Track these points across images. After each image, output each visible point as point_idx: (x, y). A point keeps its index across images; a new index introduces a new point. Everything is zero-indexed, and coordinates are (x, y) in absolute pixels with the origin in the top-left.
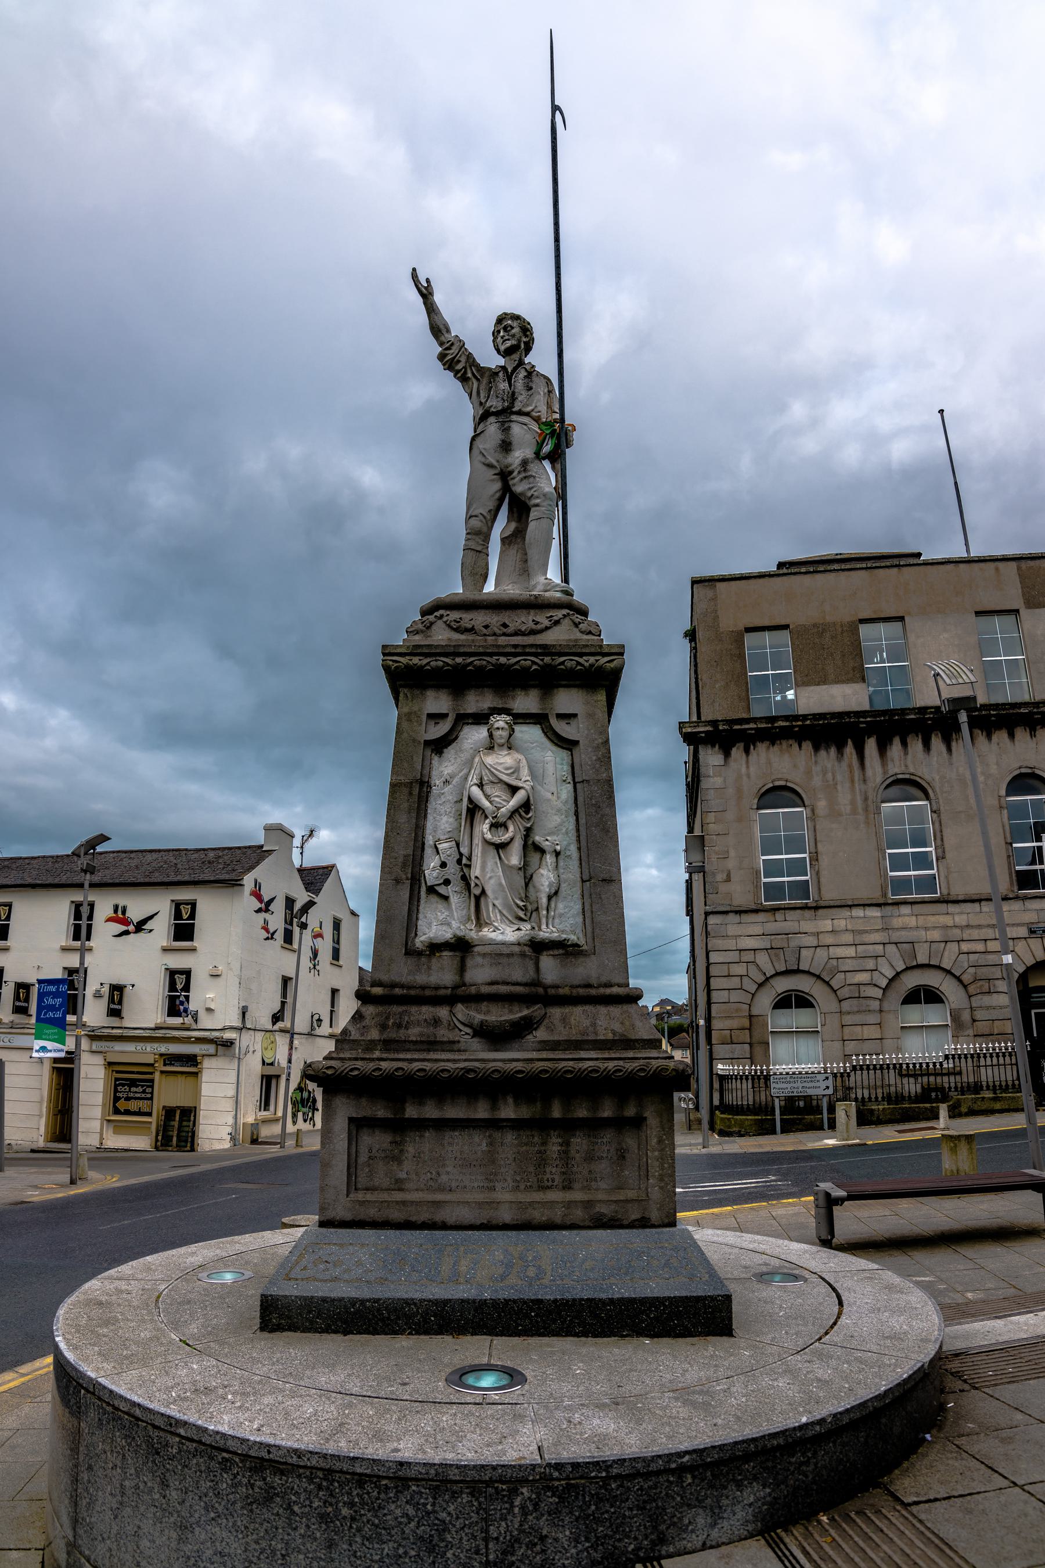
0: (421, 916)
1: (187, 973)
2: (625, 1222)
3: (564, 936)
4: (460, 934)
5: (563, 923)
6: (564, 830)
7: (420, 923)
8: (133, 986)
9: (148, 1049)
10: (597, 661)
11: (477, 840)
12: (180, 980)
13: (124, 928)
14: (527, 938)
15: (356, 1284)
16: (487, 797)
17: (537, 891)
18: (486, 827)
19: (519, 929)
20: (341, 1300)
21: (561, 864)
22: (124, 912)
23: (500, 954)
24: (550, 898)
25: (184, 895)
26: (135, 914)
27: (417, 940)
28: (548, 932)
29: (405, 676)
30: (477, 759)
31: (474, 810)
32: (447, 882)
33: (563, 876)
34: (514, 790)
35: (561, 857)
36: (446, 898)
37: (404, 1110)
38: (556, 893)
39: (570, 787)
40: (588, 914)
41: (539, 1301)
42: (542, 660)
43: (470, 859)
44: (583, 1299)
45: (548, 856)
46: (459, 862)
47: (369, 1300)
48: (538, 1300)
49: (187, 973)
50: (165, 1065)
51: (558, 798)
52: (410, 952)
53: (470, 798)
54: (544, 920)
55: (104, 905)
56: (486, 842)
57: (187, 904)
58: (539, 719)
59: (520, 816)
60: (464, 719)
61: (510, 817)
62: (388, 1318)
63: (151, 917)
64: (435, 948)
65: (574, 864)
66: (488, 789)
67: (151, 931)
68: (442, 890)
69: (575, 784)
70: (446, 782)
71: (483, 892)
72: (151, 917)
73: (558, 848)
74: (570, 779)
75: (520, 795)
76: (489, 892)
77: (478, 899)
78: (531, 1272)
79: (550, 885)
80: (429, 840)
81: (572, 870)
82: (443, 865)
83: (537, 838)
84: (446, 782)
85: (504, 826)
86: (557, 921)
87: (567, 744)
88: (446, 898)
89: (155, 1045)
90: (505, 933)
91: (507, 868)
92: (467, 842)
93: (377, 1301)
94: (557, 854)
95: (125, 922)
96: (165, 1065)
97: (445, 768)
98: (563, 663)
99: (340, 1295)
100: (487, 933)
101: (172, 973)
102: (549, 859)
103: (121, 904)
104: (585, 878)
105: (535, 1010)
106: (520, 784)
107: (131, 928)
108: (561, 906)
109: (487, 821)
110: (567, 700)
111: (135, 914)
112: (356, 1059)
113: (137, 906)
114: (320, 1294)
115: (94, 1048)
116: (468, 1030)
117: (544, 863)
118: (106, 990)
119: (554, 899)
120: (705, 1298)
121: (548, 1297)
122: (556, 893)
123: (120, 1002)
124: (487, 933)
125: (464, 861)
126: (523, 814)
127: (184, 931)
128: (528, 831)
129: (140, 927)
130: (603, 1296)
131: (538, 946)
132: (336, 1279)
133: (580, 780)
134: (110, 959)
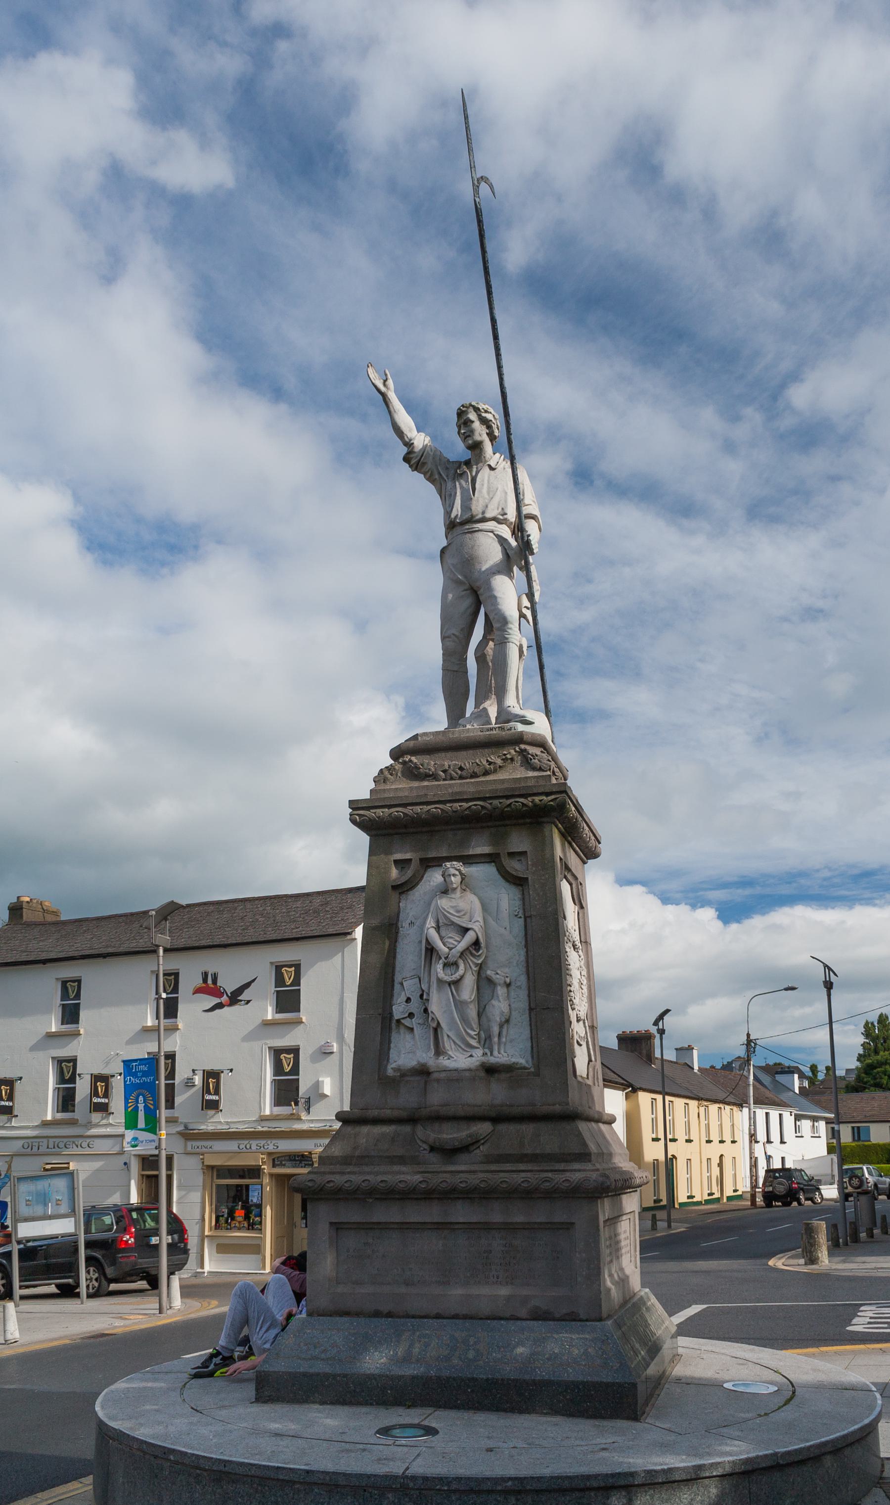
0: (392, 1045)
1: (295, 1051)
2: (557, 1316)
3: (513, 1060)
4: (423, 1061)
5: (513, 1051)
6: (515, 962)
8: (231, 1070)
9: (254, 1147)
10: (541, 801)
11: (434, 979)
12: (287, 1062)
13: (216, 1001)
14: (478, 1063)
15: (330, 1362)
16: (442, 938)
17: (489, 1021)
19: (471, 1056)
20: (318, 1374)
21: (512, 994)
22: (215, 981)
23: (456, 1078)
24: (501, 1026)
25: (285, 954)
26: (229, 984)
27: (390, 1067)
28: (500, 1057)
30: (434, 903)
31: (431, 951)
32: (411, 1015)
33: (513, 1006)
35: (513, 987)
36: (412, 1029)
38: (507, 1021)
39: (522, 919)
41: (474, 1380)
42: (491, 804)
43: (428, 994)
44: (510, 1379)
45: (499, 988)
46: (421, 996)
47: (339, 1375)
48: (473, 1379)
49: (295, 1051)
50: (274, 1166)
53: (427, 940)
54: (496, 1047)
55: (191, 971)
56: (440, 981)
57: (290, 966)
58: (492, 858)
59: (472, 954)
60: (428, 863)
62: (354, 1391)
63: (248, 985)
64: (404, 1074)
65: (523, 994)
67: (248, 1002)
68: (407, 1022)
69: (525, 918)
72: (248, 985)
75: (470, 937)
77: (436, 1030)
78: (471, 1354)
79: (502, 1013)
80: (398, 978)
82: (408, 1000)
83: (489, 972)
87: (518, 882)
88: (412, 1029)
89: (262, 1142)
90: (460, 1059)
91: (460, 1005)
92: (426, 980)
93: (345, 1376)
94: (508, 985)
95: (216, 991)
96: (274, 1166)
98: (510, 805)
99: (316, 1371)
100: (444, 1062)
101: (277, 1053)
103: (211, 972)
104: (533, 1006)
105: (484, 1128)
106: (470, 926)
107: (224, 999)
108: (511, 1032)
109: (441, 961)
110: (519, 841)
111: (229, 984)
112: (334, 1173)
113: (231, 970)
114: (302, 1370)
115: (189, 1149)
116: (425, 1146)
118: (198, 1080)
120: (613, 1384)
121: (481, 1376)
122: (507, 1021)
123: (217, 1092)
125: (425, 997)
126: (474, 952)
127: (288, 1001)
128: (481, 966)
129: (234, 999)
130: (527, 1377)
131: (490, 1070)
132: (315, 1358)
134: (202, 1038)
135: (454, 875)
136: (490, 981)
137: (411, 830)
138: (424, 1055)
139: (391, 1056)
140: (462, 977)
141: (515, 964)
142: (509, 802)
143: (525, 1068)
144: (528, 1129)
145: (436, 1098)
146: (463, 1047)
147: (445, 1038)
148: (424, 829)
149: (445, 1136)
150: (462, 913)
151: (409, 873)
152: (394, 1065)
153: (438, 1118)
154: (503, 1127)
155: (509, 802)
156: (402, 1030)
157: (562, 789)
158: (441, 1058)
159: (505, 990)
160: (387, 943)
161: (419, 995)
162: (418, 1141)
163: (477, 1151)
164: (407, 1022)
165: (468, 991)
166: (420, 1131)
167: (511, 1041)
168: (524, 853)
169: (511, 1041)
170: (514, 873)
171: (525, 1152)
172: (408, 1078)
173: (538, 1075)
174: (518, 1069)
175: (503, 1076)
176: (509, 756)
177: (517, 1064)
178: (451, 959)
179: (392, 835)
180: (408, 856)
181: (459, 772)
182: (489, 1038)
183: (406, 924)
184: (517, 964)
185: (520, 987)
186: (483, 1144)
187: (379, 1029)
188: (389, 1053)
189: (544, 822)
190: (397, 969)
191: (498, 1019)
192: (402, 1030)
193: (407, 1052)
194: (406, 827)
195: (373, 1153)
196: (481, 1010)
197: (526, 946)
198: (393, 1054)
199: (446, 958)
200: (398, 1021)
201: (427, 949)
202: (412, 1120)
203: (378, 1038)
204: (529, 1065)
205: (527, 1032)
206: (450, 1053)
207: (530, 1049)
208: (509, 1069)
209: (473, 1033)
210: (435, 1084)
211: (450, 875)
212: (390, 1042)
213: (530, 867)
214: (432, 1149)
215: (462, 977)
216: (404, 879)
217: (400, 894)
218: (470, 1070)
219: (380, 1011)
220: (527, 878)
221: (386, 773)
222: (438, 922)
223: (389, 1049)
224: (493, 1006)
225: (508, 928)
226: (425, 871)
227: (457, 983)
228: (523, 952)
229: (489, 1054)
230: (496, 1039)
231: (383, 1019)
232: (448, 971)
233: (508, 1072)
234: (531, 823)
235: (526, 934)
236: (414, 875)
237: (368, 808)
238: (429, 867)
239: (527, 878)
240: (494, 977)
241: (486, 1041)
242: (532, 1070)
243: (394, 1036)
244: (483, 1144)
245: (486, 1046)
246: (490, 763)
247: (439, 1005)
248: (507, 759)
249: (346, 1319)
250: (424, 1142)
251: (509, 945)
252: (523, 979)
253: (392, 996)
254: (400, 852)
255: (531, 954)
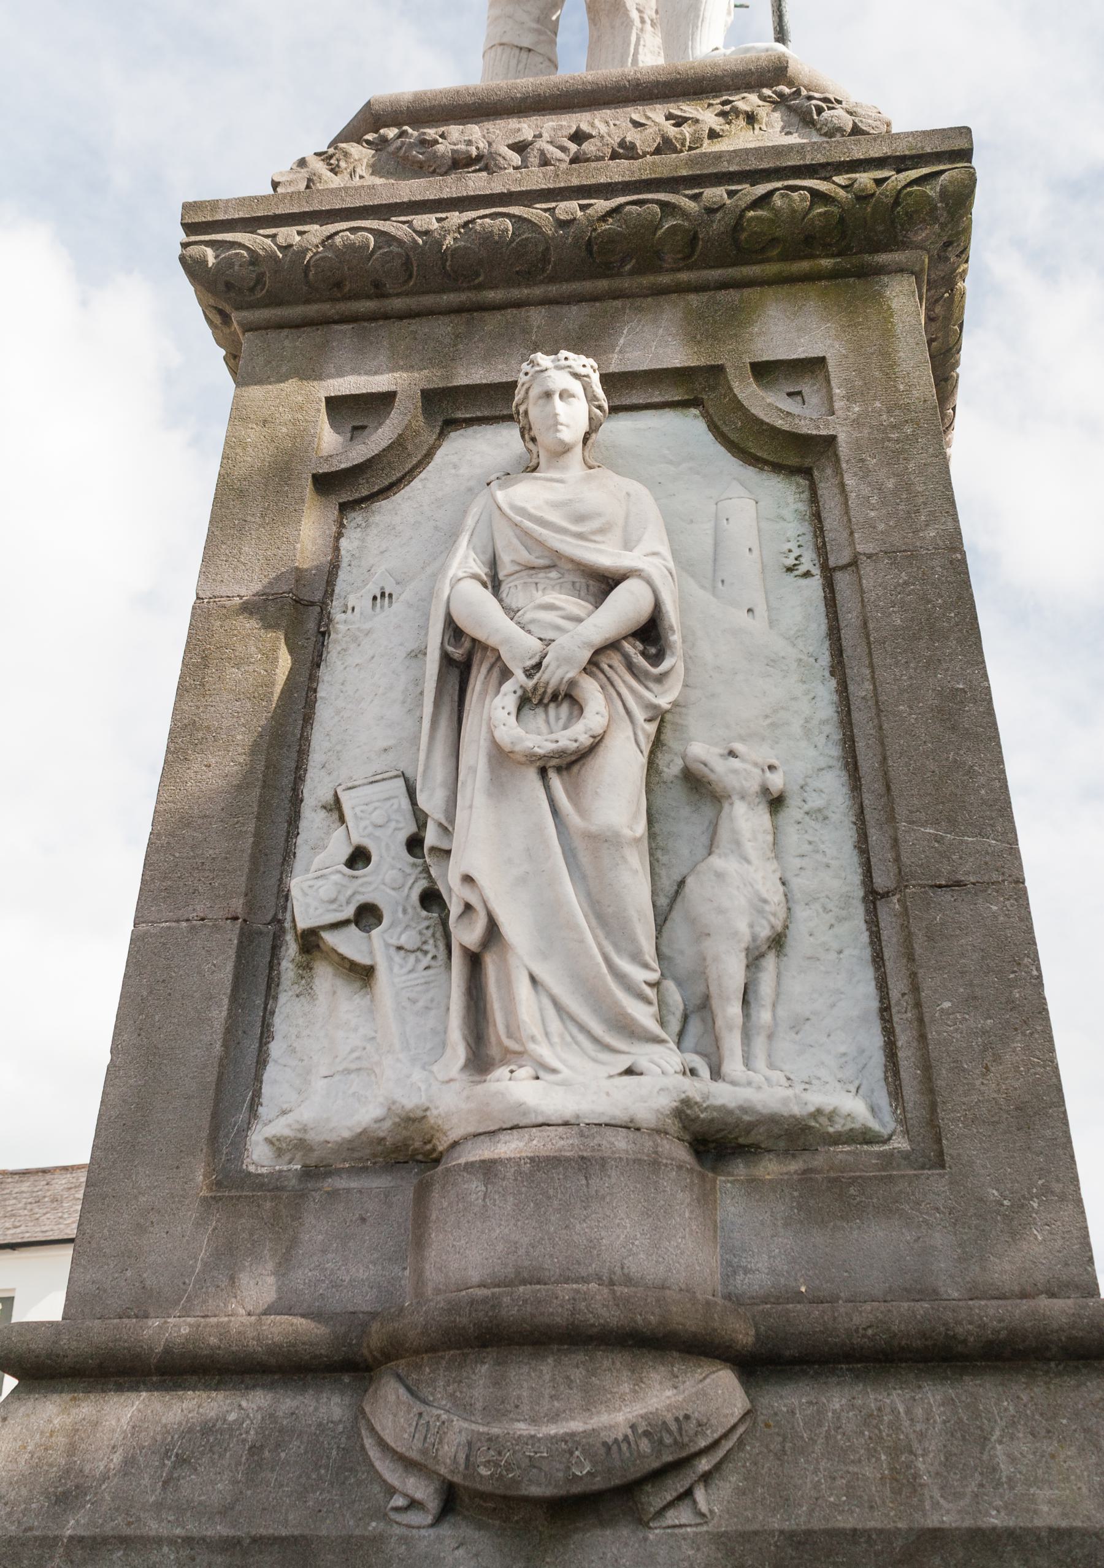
0: (276, 1048)
4: (410, 1101)
5: (813, 1059)
7: (271, 1073)
10: (879, 182)
16: (511, 612)
17: (702, 934)
18: (506, 700)
21: (792, 837)
24: (754, 961)
28: (758, 1084)
29: (265, 289)
31: (463, 661)
32: (367, 915)
33: (795, 883)
34: (603, 583)
35: (792, 811)
36: (362, 974)
37: (14, 1375)
38: (778, 942)
39: (814, 586)
40: (902, 1018)
43: (446, 831)
46: (414, 844)
51: (772, 623)
52: (232, 1186)
54: (732, 1043)
56: (502, 758)
58: (691, 388)
59: (630, 667)
61: (593, 665)
64: (317, 1169)
65: (837, 841)
66: (516, 593)
68: (348, 944)
69: (829, 574)
70: (383, 596)
71: (493, 931)
73: (776, 782)
74: (809, 561)
75: (625, 606)
76: (513, 928)
77: (474, 961)
80: (316, 789)
81: (826, 862)
82: (359, 857)
84: (383, 596)
85: (567, 697)
86: (785, 1044)
87: (795, 456)
90: (574, 1078)
91: (584, 852)
92: (440, 771)
94: (776, 803)
97: (382, 544)
100: (517, 1088)
102: (747, 820)
109: (508, 686)
110: (788, 329)
117: (724, 834)
119: (770, 962)
122: (778, 942)
124: (517, 1088)
125: (431, 838)
131: (715, 1143)
133: (845, 558)
135: (565, 395)
136: (698, 785)
137: (398, 304)
138: (418, 1075)
139: (266, 1089)
140: (596, 744)
141: (796, 728)
142: (761, 189)
143: (866, 1137)
144: (920, 1408)
145: (470, 1252)
146: (598, 1029)
147: (523, 989)
148: (449, 299)
149: (522, 1428)
150: (595, 524)
151: (380, 437)
152: (271, 1131)
153: (497, 1335)
154: (791, 1400)
155: (761, 189)
156: (324, 977)
157: (958, 144)
158: (502, 1072)
159: (762, 817)
160: (285, 661)
161: (403, 836)
162: (374, 1453)
163: (682, 1515)
164: (348, 944)
165: (617, 792)
166: (392, 1412)
167: (797, 1025)
168: (814, 366)
169: (797, 1025)
170: (779, 423)
171: (933, 1521)
172: (341, 1183)
173: (940, 1163)
174: (837, 1139)
175: (770, 1168)
176: (742, 106)
177: (832, 1116)
178: (554, 674)
179: (327, 321)
180: (380, 383)
181: (573, 147)
182: (701, 1008)
183: (359, 599)
184: (807, 733)
185: (819, 815)
186: (706, 1478)
187: (226, 974)
188: (258, 1079)
189: (881, 270)
190: (317, 756)
191: (742, 925)
192: (324, 977)
193: (342, 1065)
194: (378, 291)
195: (153, 1527)
196: (663, 901)
197: (838, 667)
198: (277, 1083)
199: (530, 672)
200: (310, 941)
201: (447, 660)
202: (348, 1362)
203: (219, 1013)
204: (884, 1123)
205: (863, 990)
206: (543, 1051)
207: (878, 1058)
208: (796, 1135)
209: (640, 976)
210: (475, 1186)
211: (548, 395)
212: (266, 1034)
213: (837, 405)
214: (452, 1501)
215: (596, 744)
216: (360, 453)
217: (344, 508)
218: (630, 1126)
219: (238, 905)
220: (832, 440)
221: (320, 167)
222: (493, 564)
223: (262, 1061)
224: (720, 876)
225: (761, 610)
226: (442, 435)
227: (571, 763)
228: (826, 691)
229: (704, 1072)
230: (734, 1010)
231: (247, 940)
232: (537, 719)
233: (789, 1153)
234: (834, 275)
235: (834, 633)
236: (398, 445)
237: (251, 224)
238: (450, 425)
239: (832, 440)
240: (721, 770)
241: (694, 1019)
242: (900, 1143)
243: (291, 1014)
244: (706, 1478)
245: (690, 1040)
246: (680, 122)
247: (495, 852)
248: (736, 112)
249: (206, 1123)
250: (409, 1464)
251: (772, 662)
252: (831, 789)
253: (288, 855)
254: (355, 371)
255: (860, 690)
